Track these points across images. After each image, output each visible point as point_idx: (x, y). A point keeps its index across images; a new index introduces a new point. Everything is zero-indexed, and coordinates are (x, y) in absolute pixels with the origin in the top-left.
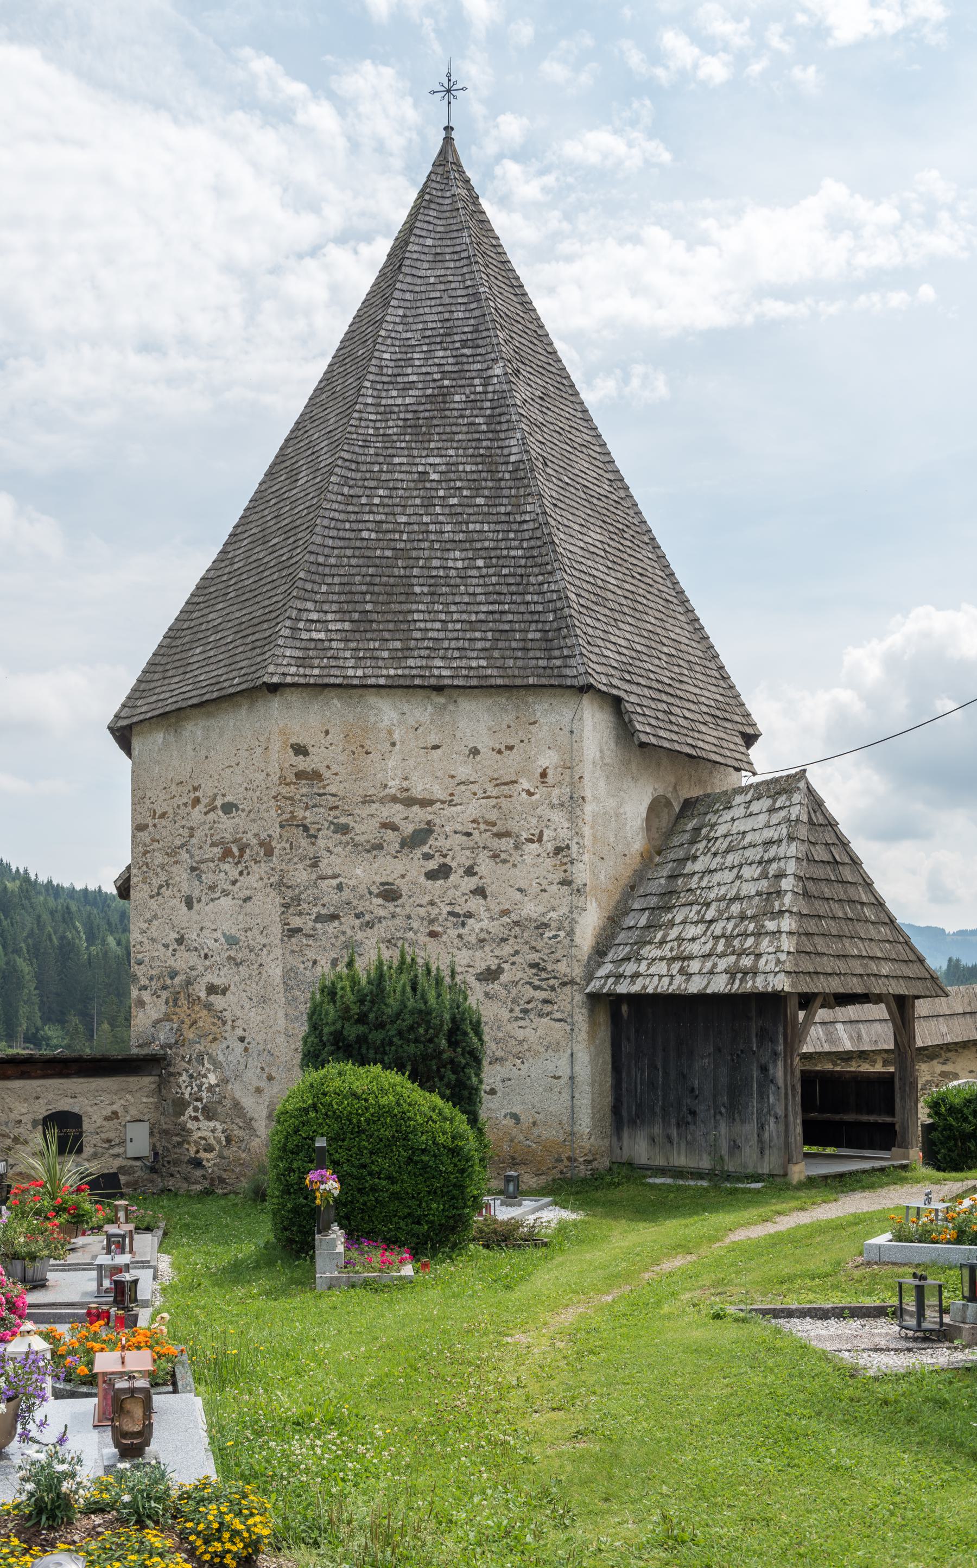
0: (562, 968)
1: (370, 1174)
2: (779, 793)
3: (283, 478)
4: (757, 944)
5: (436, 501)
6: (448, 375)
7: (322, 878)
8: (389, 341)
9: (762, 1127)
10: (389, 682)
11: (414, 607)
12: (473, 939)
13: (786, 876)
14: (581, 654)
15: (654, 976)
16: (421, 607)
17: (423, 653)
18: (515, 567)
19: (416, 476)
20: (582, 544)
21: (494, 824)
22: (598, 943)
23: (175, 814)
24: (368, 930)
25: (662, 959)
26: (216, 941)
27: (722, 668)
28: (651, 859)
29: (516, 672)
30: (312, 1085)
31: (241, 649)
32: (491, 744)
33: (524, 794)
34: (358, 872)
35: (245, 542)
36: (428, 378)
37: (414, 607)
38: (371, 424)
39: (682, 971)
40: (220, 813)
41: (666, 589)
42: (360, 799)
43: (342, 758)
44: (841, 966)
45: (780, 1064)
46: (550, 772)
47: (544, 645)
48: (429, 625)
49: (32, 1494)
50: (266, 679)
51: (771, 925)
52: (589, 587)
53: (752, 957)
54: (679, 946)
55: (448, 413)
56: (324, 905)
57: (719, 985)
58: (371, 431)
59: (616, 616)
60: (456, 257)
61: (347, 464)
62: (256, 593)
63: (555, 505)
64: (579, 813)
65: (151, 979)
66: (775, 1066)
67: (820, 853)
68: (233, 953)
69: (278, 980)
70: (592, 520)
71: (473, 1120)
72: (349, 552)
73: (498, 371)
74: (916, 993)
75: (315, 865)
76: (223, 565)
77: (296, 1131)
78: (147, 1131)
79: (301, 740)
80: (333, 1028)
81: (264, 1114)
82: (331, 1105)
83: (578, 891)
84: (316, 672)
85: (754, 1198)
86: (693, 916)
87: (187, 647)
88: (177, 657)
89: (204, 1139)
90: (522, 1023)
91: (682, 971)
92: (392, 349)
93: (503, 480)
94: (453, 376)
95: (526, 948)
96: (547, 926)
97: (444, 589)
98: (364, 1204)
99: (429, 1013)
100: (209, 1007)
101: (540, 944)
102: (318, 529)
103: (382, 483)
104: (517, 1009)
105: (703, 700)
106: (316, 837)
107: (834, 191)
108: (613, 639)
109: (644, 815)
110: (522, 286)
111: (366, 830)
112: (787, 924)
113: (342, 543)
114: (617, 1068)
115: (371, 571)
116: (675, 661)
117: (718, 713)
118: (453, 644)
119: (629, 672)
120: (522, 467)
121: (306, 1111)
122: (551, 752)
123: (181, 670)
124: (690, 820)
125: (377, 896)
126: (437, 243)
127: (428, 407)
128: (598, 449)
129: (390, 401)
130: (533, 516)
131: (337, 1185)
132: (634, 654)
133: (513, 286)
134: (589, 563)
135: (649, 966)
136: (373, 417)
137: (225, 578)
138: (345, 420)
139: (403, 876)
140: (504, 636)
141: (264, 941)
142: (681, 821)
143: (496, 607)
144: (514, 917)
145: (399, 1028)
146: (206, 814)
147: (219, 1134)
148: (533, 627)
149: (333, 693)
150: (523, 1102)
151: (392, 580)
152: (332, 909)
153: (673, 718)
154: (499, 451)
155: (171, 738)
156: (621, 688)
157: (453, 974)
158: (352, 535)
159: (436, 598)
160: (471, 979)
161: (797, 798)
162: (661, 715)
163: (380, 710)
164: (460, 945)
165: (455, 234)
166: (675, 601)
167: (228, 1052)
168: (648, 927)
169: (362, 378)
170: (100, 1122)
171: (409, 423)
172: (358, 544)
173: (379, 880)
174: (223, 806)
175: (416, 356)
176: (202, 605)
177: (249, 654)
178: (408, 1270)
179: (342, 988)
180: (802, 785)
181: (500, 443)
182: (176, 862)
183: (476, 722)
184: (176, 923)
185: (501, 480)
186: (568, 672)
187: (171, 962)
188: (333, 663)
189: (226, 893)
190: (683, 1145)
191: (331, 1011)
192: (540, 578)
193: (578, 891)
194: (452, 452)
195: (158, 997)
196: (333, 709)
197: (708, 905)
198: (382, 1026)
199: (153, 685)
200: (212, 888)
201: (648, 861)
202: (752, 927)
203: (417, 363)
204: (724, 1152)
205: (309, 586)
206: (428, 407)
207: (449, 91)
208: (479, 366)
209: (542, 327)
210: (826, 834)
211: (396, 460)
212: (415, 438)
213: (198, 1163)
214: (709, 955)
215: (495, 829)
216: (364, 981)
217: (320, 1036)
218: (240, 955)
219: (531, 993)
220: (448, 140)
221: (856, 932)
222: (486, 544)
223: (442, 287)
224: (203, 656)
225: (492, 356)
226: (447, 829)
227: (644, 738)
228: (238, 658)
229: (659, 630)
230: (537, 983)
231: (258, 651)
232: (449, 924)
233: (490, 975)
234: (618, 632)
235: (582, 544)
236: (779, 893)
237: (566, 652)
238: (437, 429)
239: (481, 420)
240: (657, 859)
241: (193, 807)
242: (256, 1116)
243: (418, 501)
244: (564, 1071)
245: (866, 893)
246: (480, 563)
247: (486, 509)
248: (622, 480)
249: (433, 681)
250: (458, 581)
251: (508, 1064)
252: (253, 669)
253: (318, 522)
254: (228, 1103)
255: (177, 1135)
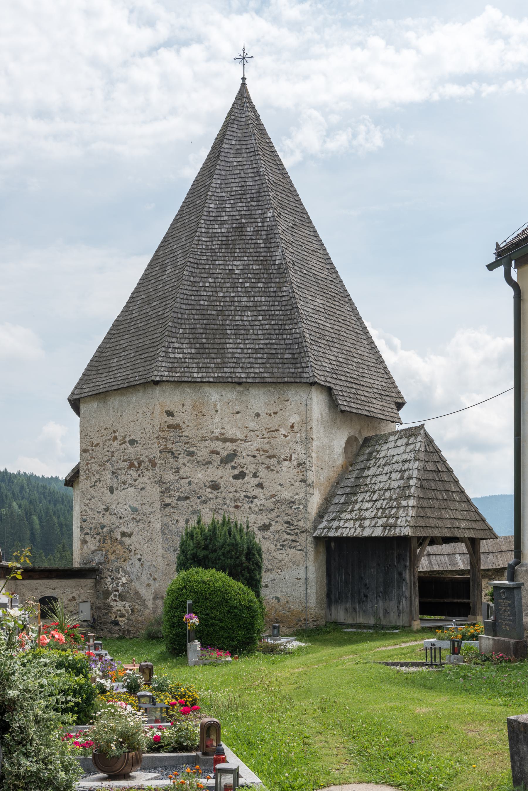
0: (301, 524)
1: (211, 618)
2: (411, 436)
3: (158, 268)
4: (397, 512)
5: (238, 285)
6: (244, 217)
7: (181, 478)
8: (213, 198)
9: (399, 603)
10: (215, 380)
11: (227, 341)
12: (257, 509)
13: (412, 478)
14: (311, 366)
15: (347, 528)
16: (231, 341)
17: (232, 365)
18: (278, 320)
19: (227, 271)
20: (312, 307)
21: (267, 451)
22: (319, 511)
23: (104, 444)
24: (204, 505)
25: (351, 519)
26: (126, 510)
27: (386, 368)
28: (347, 469)
29: (279, 375)
30: (184, 578)
31: (139, 361)
32: (266, 411)
33: (282, 436)
34: (199, 475)
35: (139, 302)
36: (234, 218)
37: (227, 341)
38: (204, 243)
39: (361, 526)
40: (128, 445)
41: (357, 327)
42: (200, 439)
43: (191, 418)
44: (439, 523)
45: (408, 571)
46: (295, 425)
47: (292, 361)
48: (235, 351)
49: (128, 683)
50: (153, 378)
51: (404, 503)
52: (316, 330)
53: (394, 519)
54: (360, 513)
55: (244, 237)
56: (182, 492)
57: (378, 532)
58: (204, 247)
59: (330, 344)
60: (248, 151)
61: (192, 265)
62: (146, 331)
63: (299, 287)
64: (310, 446)
65: (91, 529)
66: (406, 572)
67: (430, 467)
68: (135, 516)
69: (159, 530)
70: (318, 293)
71: (258, 595)
72: (194, 312)
73: (270, 215)
74: (479, 537)
75: (177, 472)
76: (127, 314)
77: (177, 599)
78: (90, 607)
79: (170, 409)
80: (192, 552)
81: (151, 597)
82: (193, 586)
83: (310, 485)
84: (178, 374)
85: (393, 636)
86: (367, 498)
87: (109, 357)
88: (104, 363)
89: (120, 611)
90: (281, 552)
91: (361, 526)
92: (215, 202)
93: (272, 274)
94: (246, 217)
95: (283, 514)
96: (294, 503)
97: (243, 332)
98: (208, 631)
99: (237, 545)
100: (122, 543)
101: (290, 512)
102: (178, 300)
103: (210, 275)
104: (279, 544)
105: (375, 386)
106: (178, 458)
107: (492, 13)
108: (328, 356)
109: (344, 446)
110: (282, 164)
111: (203, 454)
112: (412, 502)
113: (190, 307)
114: (329, 574)
115: (205, 322)
116: (360, 366)
117: (383, 392)
118: (247, 360)
119: (336, 374)
120: (282, 267)
121: (181, 589)
122: (296, 416)
123: (107, 370)
124: (368, 448)
125: (208, 487)
126: (238, 143)
127: (233, 234)
128: (322, 252)
129: (214, 231)
130: (288, 293)
131: (197, 620)
132: (339, 364)
133: (277, 165)
134: (316, 316)
135: (345, 523)
136: (205, 239)
137: (128, 321)
138: (190, 240)
139: (221, 478)
140: (272, 356)
141: (151, 510)
142: (363, 448)
143: (268, 341)
144: (277, 498)
145: (223, 552)
146: (120, 445)
147: (127, 608)
148: (287, 351)
149: (186, 385)
150: (282, 591)
151: (216, 327)
152: (186, 494)
153: (358, 397)
154: (270, 258)
155: (102, 405)
156: (332, 382)
157: (248, 527)
158: (195, 303)
159: (238, 336)
160: (256, 530)
161: (419, 438)
162: (352, 396)
163: (210, 394)
164: (250, 512)
165: (247, 138)
166: (362, 333)
167: (132, 566)
168: (344, 503)
169: (199, 217)
170: (67, 602)
171: (224, 242)
172: (198, 307)
173: (209, 480)
174: (130, 441)
175: (227, 206)
176: (116, 335)
177: (143, 364)
178: (229, 659)
179: (197, 533)
180: (422, 432)
181: (271, 254)
182: (104, 469)
183: (258, 400)
184: (104, 500)
185: (271, 274)
186: (304, 375)
187: (102, 520)
188: (186, 370)
189: (131, 485)
190: (361, 612)
191: (191, 544)
192: (291, 326)
193: (310, 485)
194: (246, 259)
195: (95, 538)
196: (187, 393)
197: (374, 492)
198: (215, 551)
199: (91, 377)
200: (124, 483)
201: (345, 470)
202: (395, 503)
203: (228, 210)
204: (381, 615)
205: (174, 330)
206: (233, 234)
207: (244, 58)
208: (260, 212)
209: (293, 186)
210: (434, 457)
211: (217, 263)
212: (227, 251)
213: (116, 623)
214: (374, 518)
215: (268, 454)
216: (207, 530)
217: (186, 555)
218: (139, 517)
219: (286, 536)
220: (244, 85)
221: (448, 506)
222: (264, 308)
223: (240, 168)
224: (119, 364)
225: (267, 206)
226: (244, 454)
227: (343, 408)
228: (137, 366)
229: (352, 350)
230: (289, 531)
231: (148, 363)
232: (245, 502)
233: (265, 527)
234: (330, 353)
235: (312, 307)
236: (409, 487)
237: (303, 365)
238: (238, 246)
239: (261, 241)
240: (350, 468)
241: (114, 441)
242: (147, 598)
243: (229, 285)
244: (302, 576)
245: (455, 486)
246: (260, 318)
247: (263, 289)
248: (334, 268)
249: (237, 380)
250: (249, 327)
251: (274, 572)
252: (146, 372)
253: (178, 296)
254: (132, 592)
255: (105, 609)
